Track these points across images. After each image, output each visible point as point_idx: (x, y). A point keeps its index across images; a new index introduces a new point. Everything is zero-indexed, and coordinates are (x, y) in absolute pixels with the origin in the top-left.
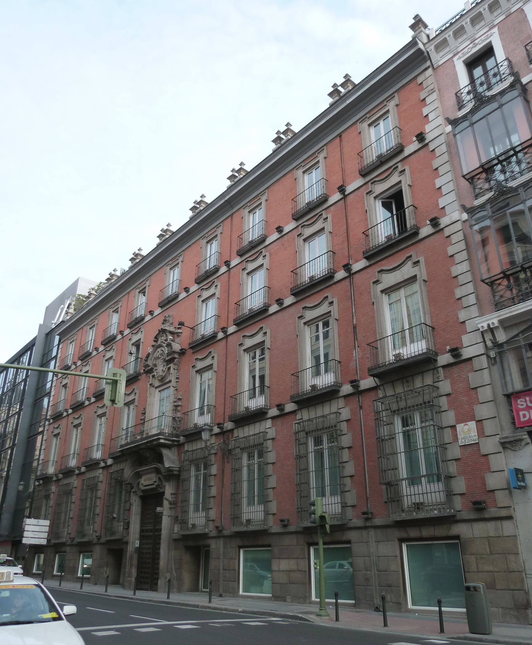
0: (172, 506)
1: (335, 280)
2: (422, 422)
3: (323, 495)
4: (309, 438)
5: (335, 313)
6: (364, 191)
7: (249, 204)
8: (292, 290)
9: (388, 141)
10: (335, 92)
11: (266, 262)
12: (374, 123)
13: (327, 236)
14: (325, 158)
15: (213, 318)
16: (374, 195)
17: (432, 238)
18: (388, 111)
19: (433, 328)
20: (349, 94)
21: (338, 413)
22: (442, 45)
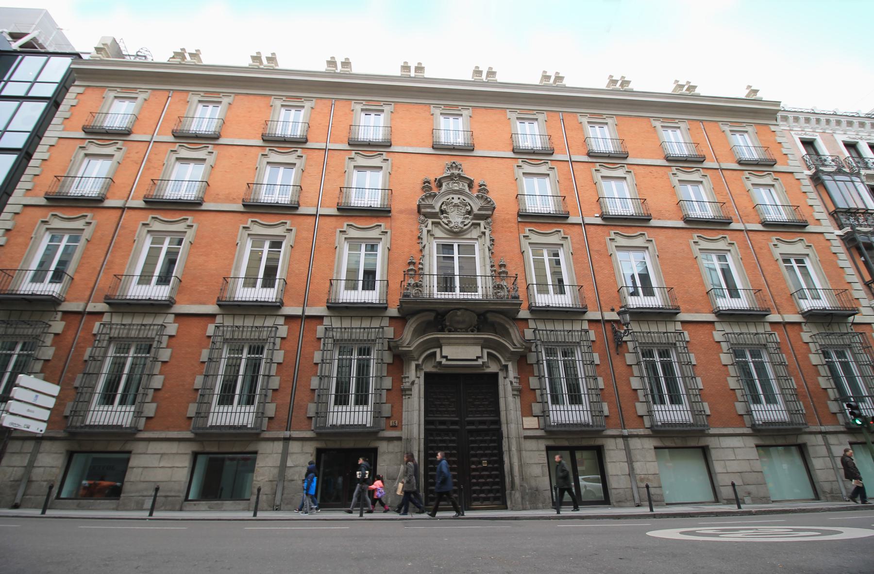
0: (515, 393)
1: (298, 212)
2: (22, 350)
3: (345, 402)
4: (112, 345)
5: (87, 233)
6: (79, 143)
7: (119, 90)
8: (46, 193)
9: (294, 128)
10: (181, 54)
11: (118, 155)
12: (287, 107)
13: (205, 170)
14: (145, 100)
15: (102, 181)
16: (178, 156)
17: (137, 212)
18: (220, 102)
19: (181, 281)
20: (414, 79)
21: (163, 327)
22: (785, 118)
